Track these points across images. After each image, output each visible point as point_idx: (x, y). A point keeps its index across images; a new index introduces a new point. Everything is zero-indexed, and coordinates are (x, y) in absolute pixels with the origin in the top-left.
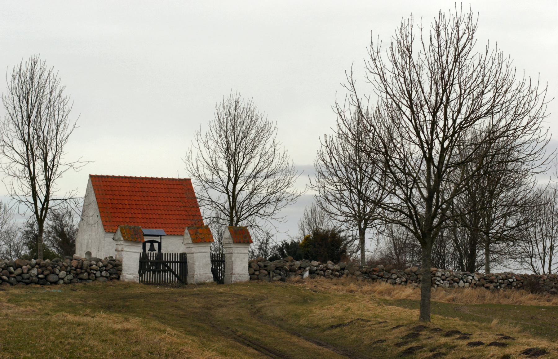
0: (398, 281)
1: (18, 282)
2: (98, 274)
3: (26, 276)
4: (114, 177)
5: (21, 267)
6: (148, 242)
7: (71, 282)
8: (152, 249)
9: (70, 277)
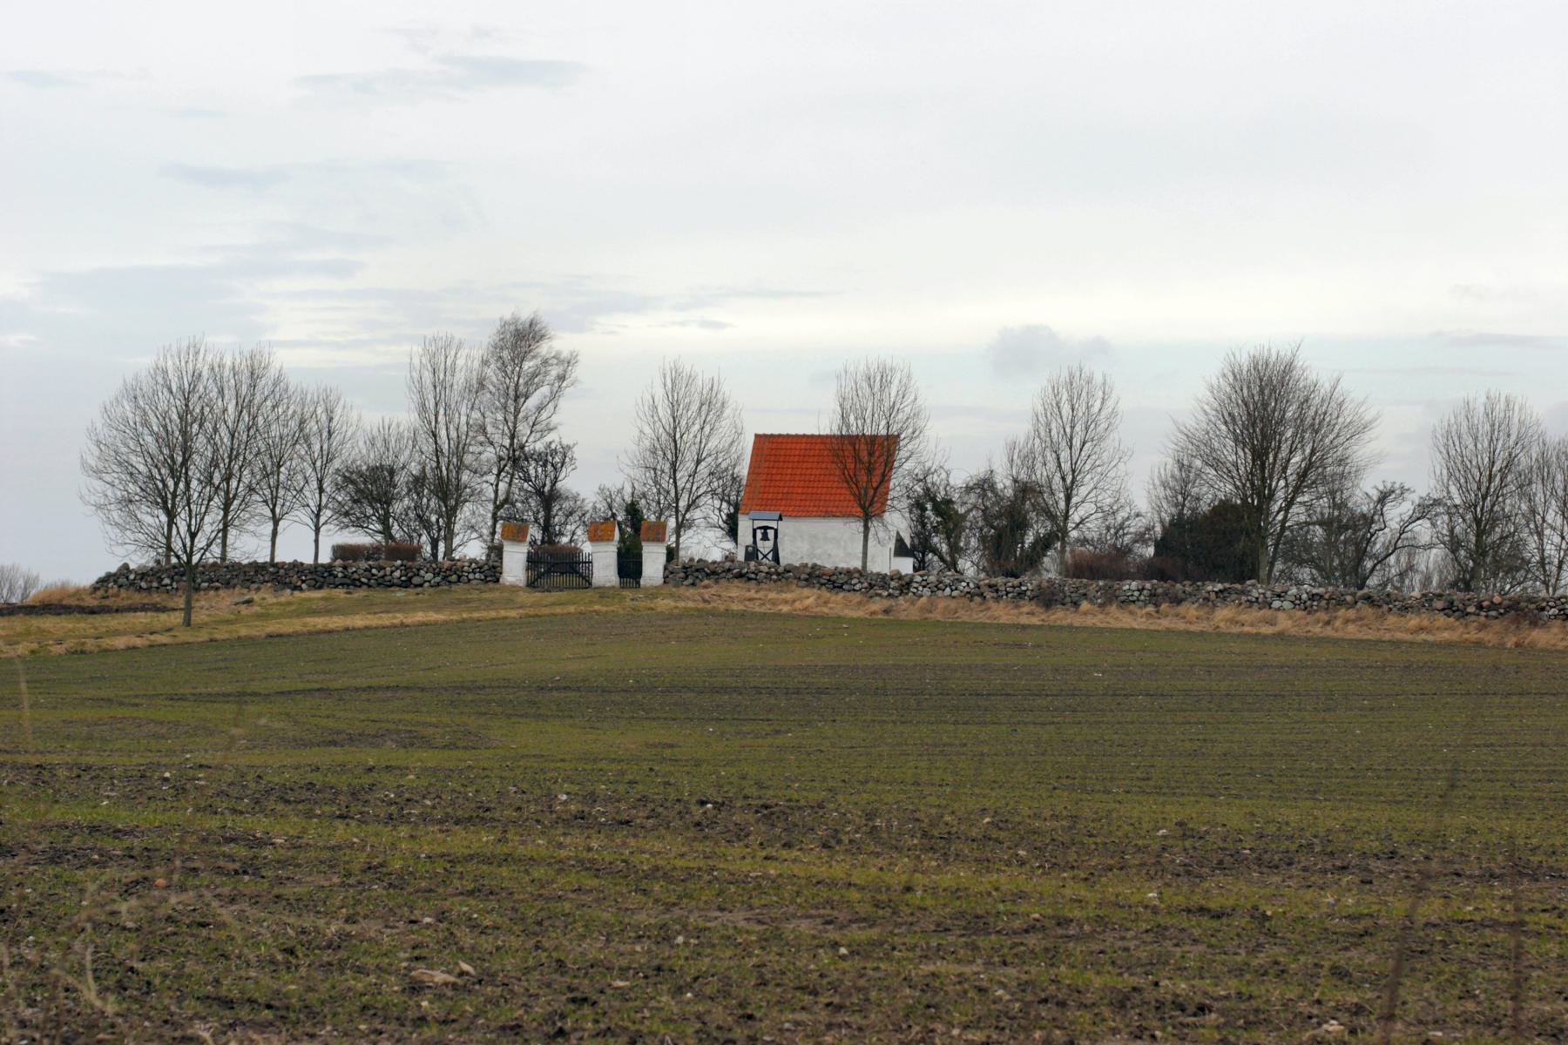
0: (857, 587)
1: (379, 584)
2: (471, 576)
3: (387, 578)
4: (788, 436)
5: (384, 568)
6: (760, 528)
7: (438, 584)
8: (765, 538)
9: (438, 579)
